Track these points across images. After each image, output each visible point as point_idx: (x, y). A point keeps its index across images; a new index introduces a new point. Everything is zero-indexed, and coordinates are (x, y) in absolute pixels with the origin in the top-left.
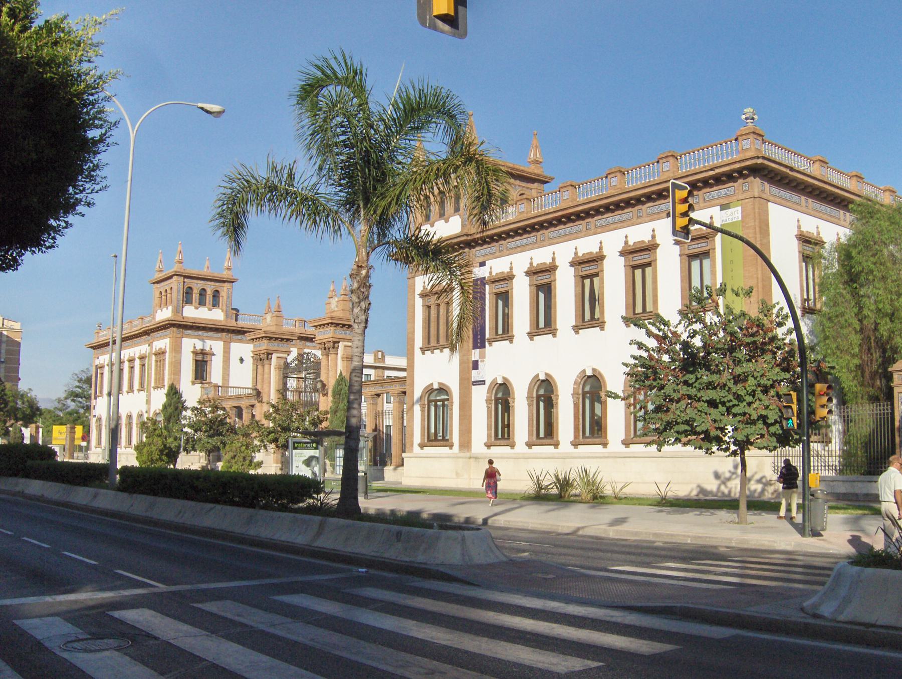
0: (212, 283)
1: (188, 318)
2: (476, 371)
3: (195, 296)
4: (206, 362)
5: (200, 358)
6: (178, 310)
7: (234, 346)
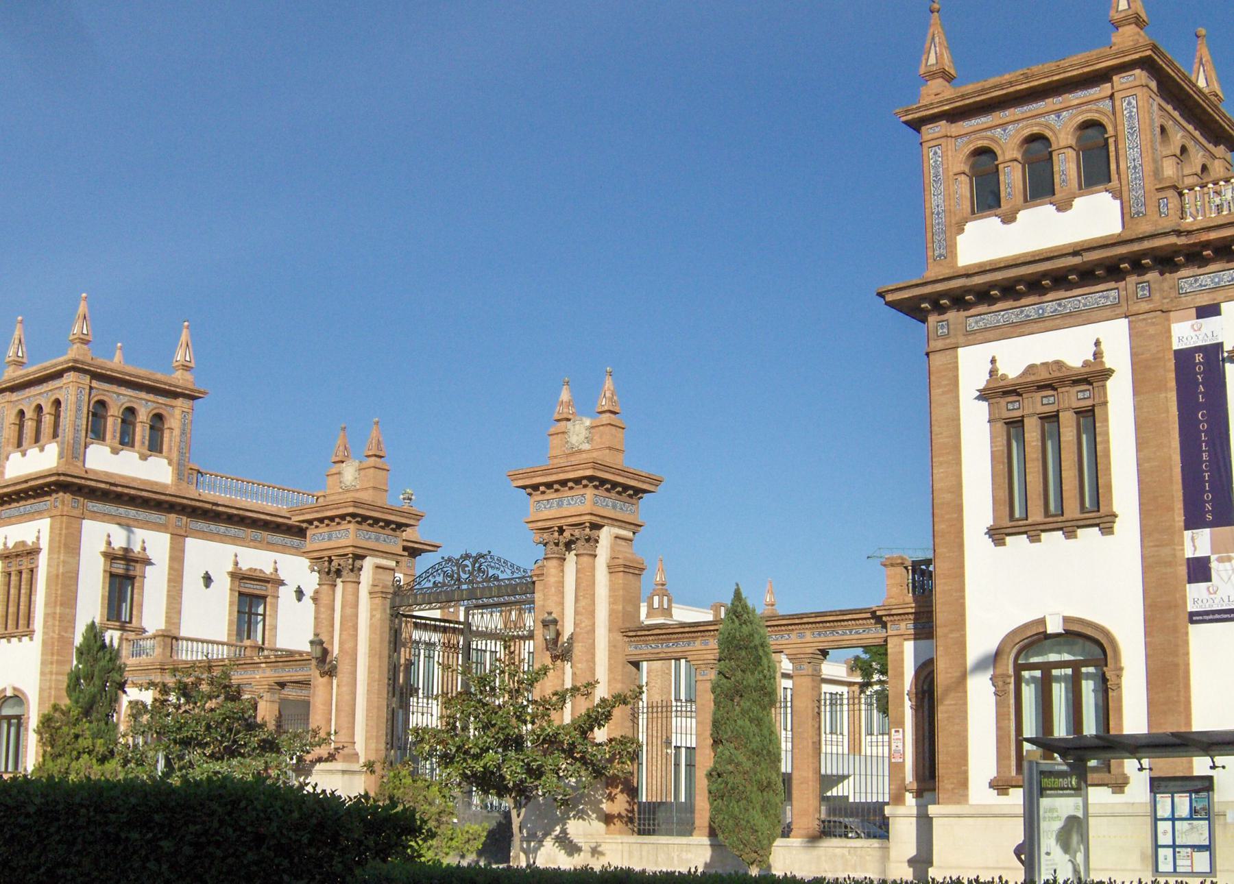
0: (151, 397)
1: (95, 472)
2: (1203, 586)
3: (112, 424)
4: (131, 579)
5: (119, 568)
6: (75, 453)
7: (193, 546)
